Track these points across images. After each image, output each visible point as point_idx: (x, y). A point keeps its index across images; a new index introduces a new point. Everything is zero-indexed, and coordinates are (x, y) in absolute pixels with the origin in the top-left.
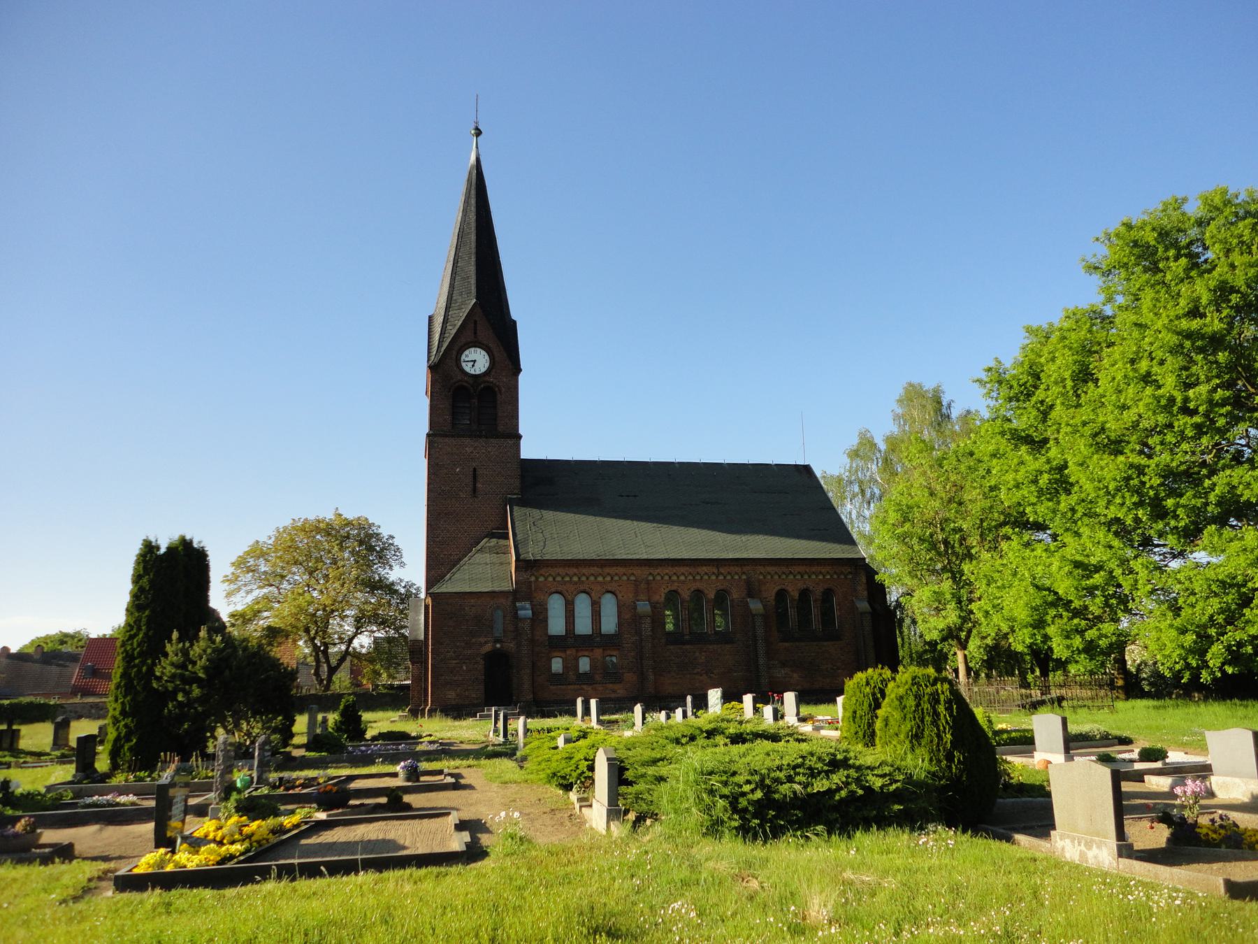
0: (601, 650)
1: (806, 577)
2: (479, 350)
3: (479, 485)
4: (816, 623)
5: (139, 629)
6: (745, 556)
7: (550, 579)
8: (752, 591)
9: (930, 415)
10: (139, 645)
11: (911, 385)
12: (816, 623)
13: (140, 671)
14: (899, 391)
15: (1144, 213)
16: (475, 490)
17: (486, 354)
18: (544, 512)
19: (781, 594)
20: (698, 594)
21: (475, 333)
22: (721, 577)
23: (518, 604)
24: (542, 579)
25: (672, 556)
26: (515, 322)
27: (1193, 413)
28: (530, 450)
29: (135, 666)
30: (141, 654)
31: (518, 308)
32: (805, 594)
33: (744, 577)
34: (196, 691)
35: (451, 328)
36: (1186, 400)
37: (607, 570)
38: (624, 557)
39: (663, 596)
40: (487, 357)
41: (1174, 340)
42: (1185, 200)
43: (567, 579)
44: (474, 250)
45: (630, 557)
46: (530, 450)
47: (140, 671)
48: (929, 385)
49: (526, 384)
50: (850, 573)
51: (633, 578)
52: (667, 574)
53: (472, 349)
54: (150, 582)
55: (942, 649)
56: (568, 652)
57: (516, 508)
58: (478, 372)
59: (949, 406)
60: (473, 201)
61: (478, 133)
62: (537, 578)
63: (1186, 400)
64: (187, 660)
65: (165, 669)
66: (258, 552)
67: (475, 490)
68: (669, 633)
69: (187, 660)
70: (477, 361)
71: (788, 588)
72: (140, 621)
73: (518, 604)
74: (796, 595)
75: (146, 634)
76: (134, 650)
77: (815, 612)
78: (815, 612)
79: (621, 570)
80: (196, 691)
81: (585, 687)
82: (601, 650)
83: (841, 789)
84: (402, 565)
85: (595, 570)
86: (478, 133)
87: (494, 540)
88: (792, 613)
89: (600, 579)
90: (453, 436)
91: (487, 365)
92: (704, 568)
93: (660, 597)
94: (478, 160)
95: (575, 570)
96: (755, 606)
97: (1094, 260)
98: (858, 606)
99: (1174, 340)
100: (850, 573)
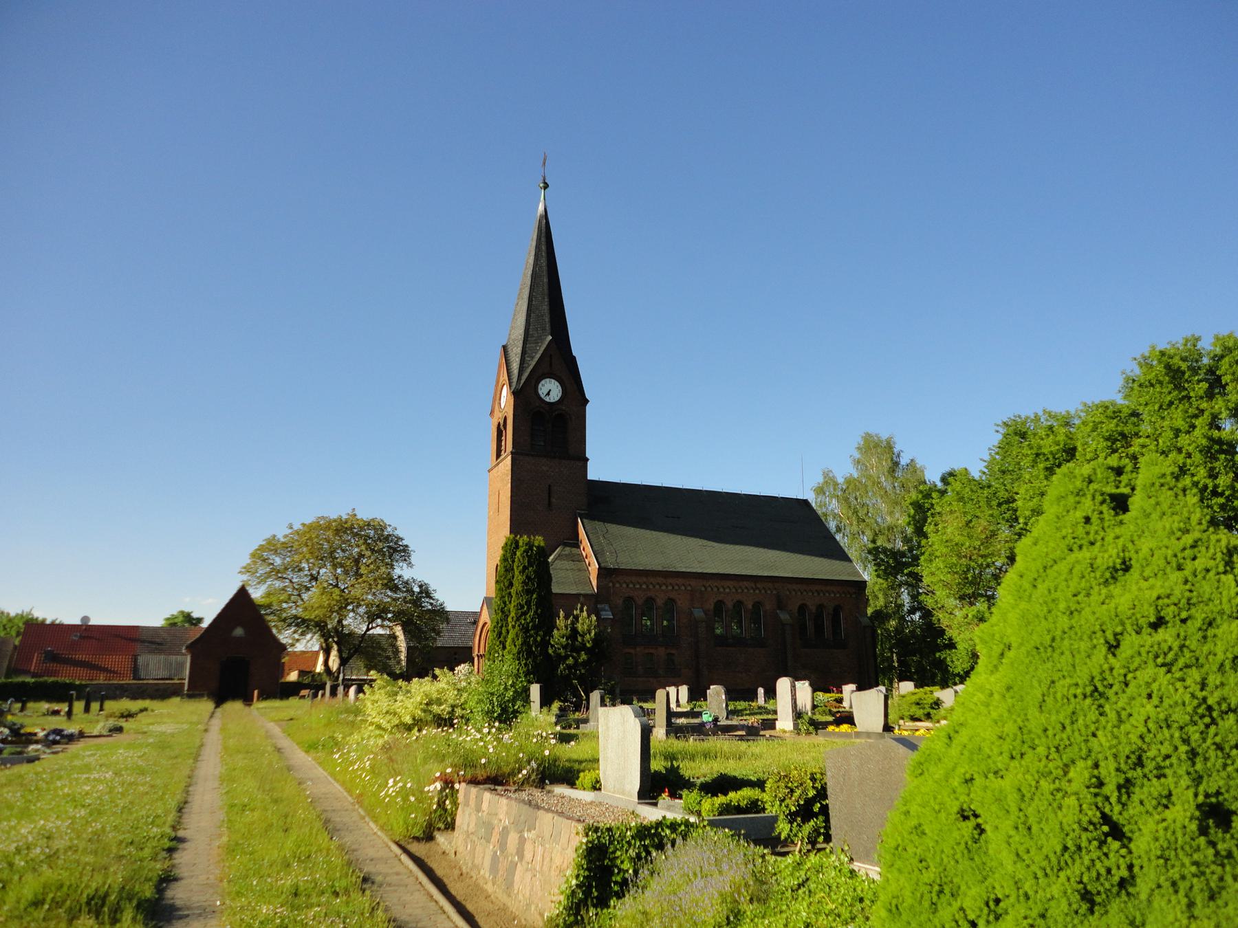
0: (663, 649)
1: (822, 595)
2: (553, 381)
3: (553, 500)
4: (828, 632)
5: (529, 608)
6: (777, 575)
7: (624, 585)
8: (781, 605)
9: (886, 464)
10: (532, 620)
11: (867, 434)
12: (828, 632)
13: (535, 640)
14: (858, 440)
15: (1168, 343)
16: (550, 503)
17: (558, 384)
18: (609, 526)
19: (802, 608)
20: (739, 604)
21: (551, 365)
22: (757, 592)
23: (599, 606)
24: (617, 585)
25: (721, 571)
26: (575, 358)
27: (1222, 494)
28: (595, 472)
29: (531, 636)
30: (534, 627)
31: (578, 348)
32: (820, 607)
33: (774, 592)
34: (584, 656)
35: (528, 359)
36: (1216, 486)
37: (670, 581)
38: (684, 570)
39: (713, 604)
40: (560, 388)
41: (1204, 442)
42: (1198, 339)
43: (638, 586)
44: (546, 291)
45: (688, 570)
46: (595, 472)
47: (535, 640)
48: (884, 436)
49: (592, 413)
50: (855, 593)
51: (689, 588)
52: (645, 583)
53: (548, 380)
54: (535, 572)
55: (940, 656)
56: (638, 649)
57: (585, 520)
58: (552, 401)
59: (899, 456)
60: (544, 248)
61: (546, 186)
62: (614, 585)
63: (1216, 486)
64: (574, 633)
65: (558, 636)
66: (272, 546)
67: (550, 503)
68: (717, 636)
69: (574, 633)
70: (551, 390)
71: (808, 603)
72: (530, 602)
73: (599, 606)
74: (813, 609)
75: (536, 612)
76: (528, 624)
77: (827, 623)
78: (827, 623)
79: (680, 581)
80: (584, 656)
81: (651, 679)
82: (663, 649)
83: (66, 900)
84: (410, 565)
85: (660, 580)
86: (546, 186)
87: (568, 549)
88: (810, 625)
89: (664, 587)
90: (532, 456)
91: (560, 395)
92: (745, 583)
93: (710, 605)
94: (545, 209)
95: (645, 579)
96: (784, 616)
97: (1131, 374)
98: (861, 620)
99: (1204, 442)
100: (855, 593)
